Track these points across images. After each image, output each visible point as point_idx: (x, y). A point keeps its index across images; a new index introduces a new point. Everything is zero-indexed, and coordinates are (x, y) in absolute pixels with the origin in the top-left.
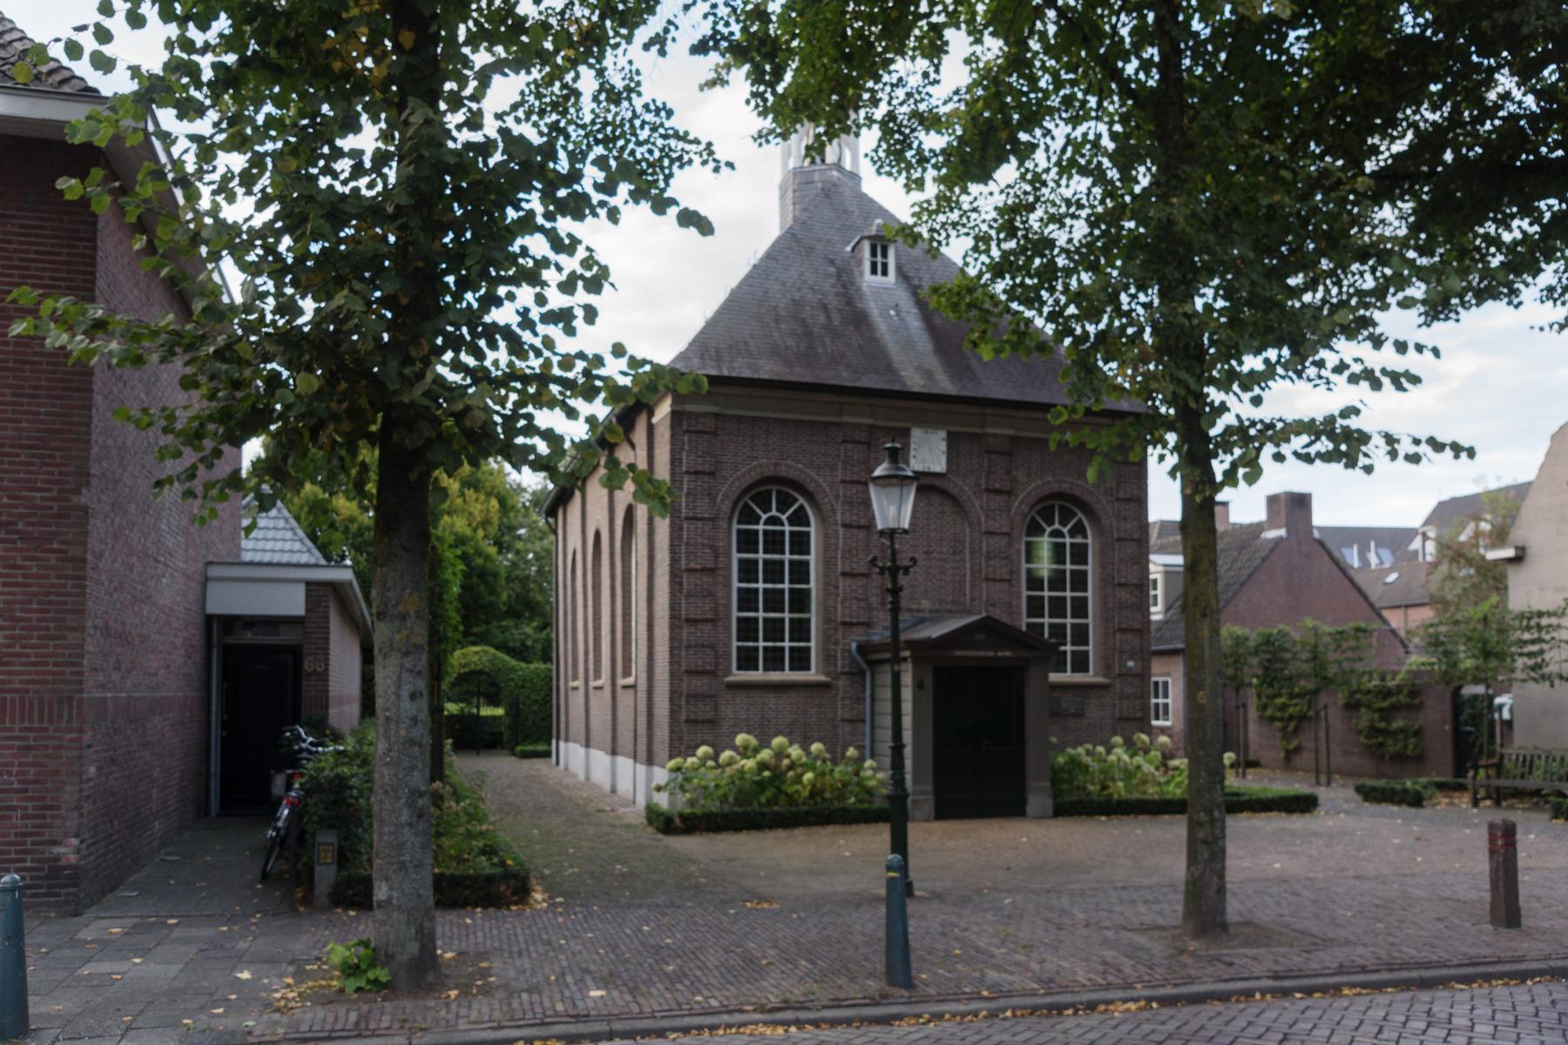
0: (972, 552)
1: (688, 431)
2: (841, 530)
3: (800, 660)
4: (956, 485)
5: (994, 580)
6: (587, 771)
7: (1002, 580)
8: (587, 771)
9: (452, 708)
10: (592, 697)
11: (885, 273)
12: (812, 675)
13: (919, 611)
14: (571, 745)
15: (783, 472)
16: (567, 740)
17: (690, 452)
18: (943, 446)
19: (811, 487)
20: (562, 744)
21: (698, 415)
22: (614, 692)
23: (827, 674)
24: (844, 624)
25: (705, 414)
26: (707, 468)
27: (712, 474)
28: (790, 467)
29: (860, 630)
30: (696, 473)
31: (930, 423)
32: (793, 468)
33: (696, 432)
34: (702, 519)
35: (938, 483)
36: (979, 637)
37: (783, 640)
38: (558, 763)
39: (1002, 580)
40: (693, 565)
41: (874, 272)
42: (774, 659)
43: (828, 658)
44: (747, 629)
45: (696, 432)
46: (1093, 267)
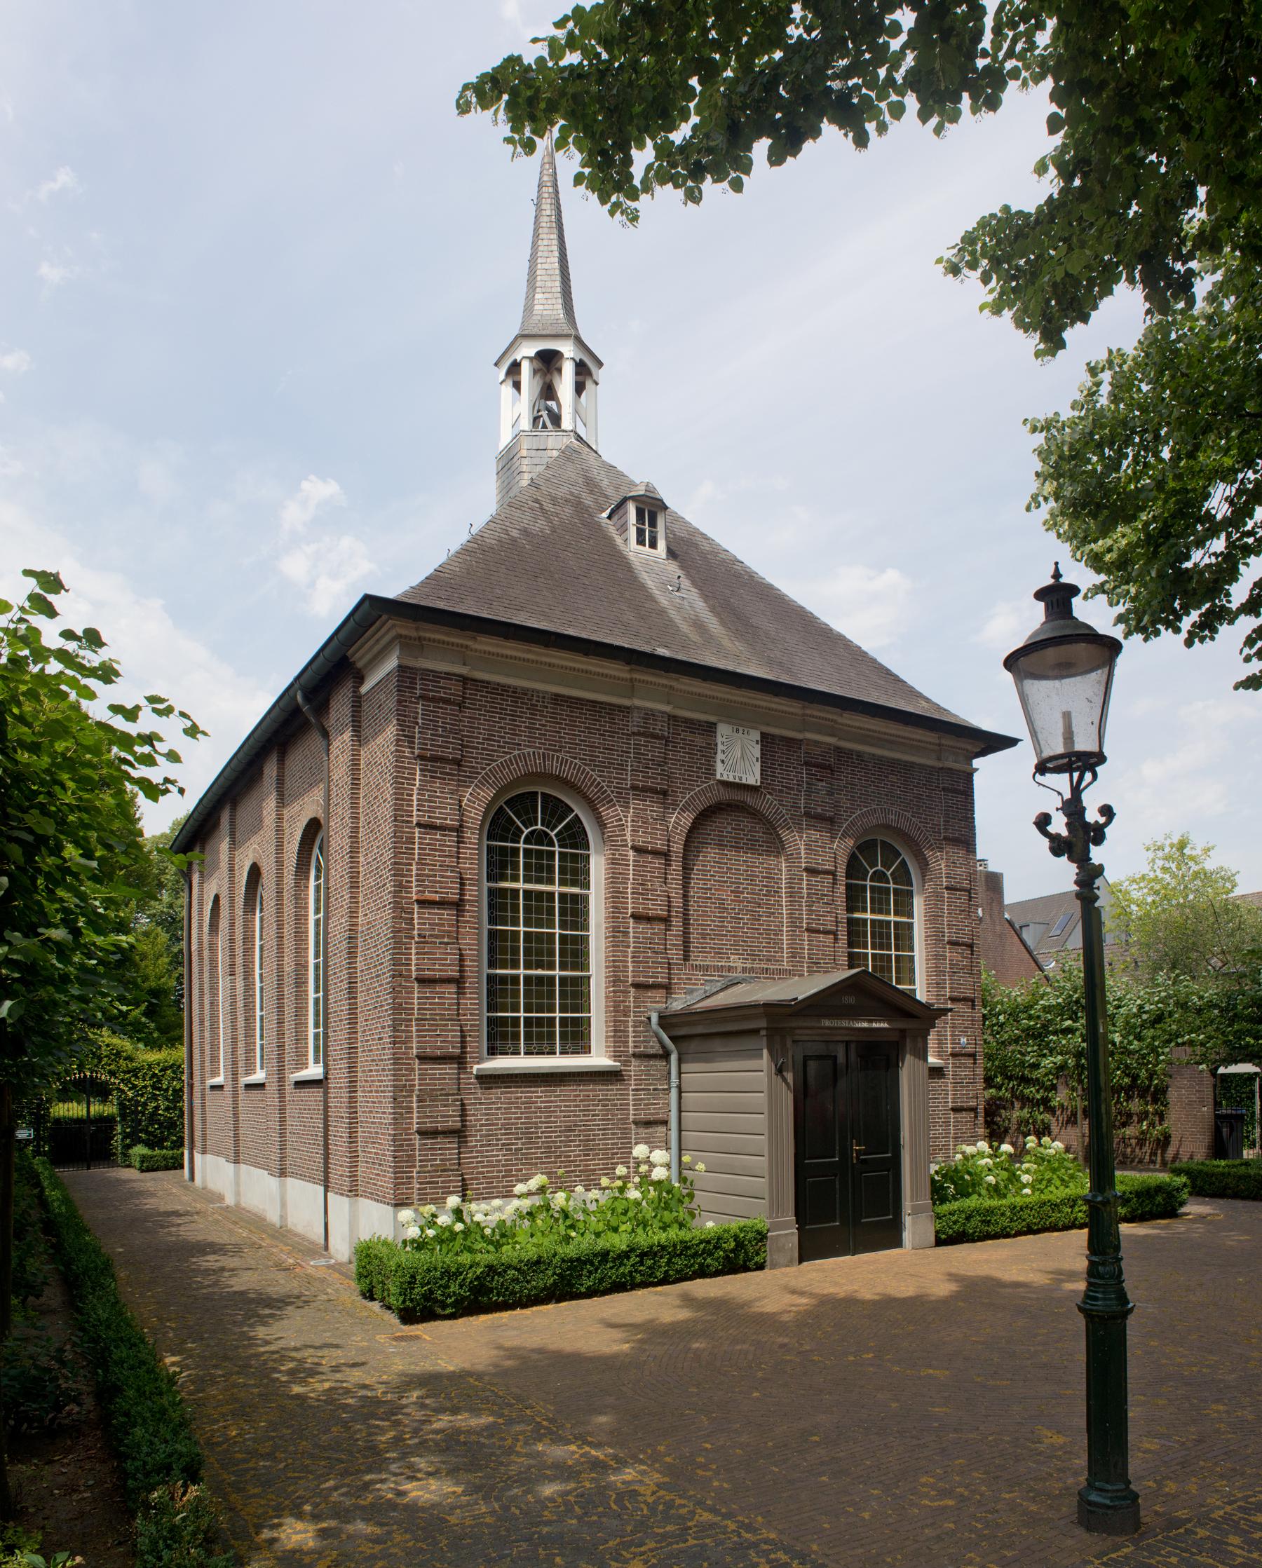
0: (791, 894)
1: (423, 697)
2: (631, 853)
3: (576, 1038)
4: (767, 804)
5: (818, 932)
6: (238, 1194)
7: (826, 932)
8: (238, 1194)
9: (1157, 1166)
10: (241, 1097)
11: (653, 545)
12: (598, 1058)
13: (730, 969)
14: (209, 1157)
15: (554, 767)
16: (204, 1152)
17: (425, 727)
18: (756, 751)
19: (592, 792)
20: (198, 1157)
21: (438, 676)
22: (281, 1089)
23: (616, 1057)
24: (637, 986)
25: (449, 676)
26: (451, 753)
27: (458, 763)
28: (563, 762)
29: (659, 994)
30: (434, 759)
31: (740, 718)
32: (565, 764)
33: (434, 700)
34: (441, 828)
35: (749, 799)
36: (848, 1000)
37: (555, 1012)
38: (192, 1178)
39: (826, 932)
40: (428, 896)
41: (641, 541)
42: (540, 1041)
43: (617, 1034)
44: (498, 990)
45: (434, 700)
46: (1122, 400)
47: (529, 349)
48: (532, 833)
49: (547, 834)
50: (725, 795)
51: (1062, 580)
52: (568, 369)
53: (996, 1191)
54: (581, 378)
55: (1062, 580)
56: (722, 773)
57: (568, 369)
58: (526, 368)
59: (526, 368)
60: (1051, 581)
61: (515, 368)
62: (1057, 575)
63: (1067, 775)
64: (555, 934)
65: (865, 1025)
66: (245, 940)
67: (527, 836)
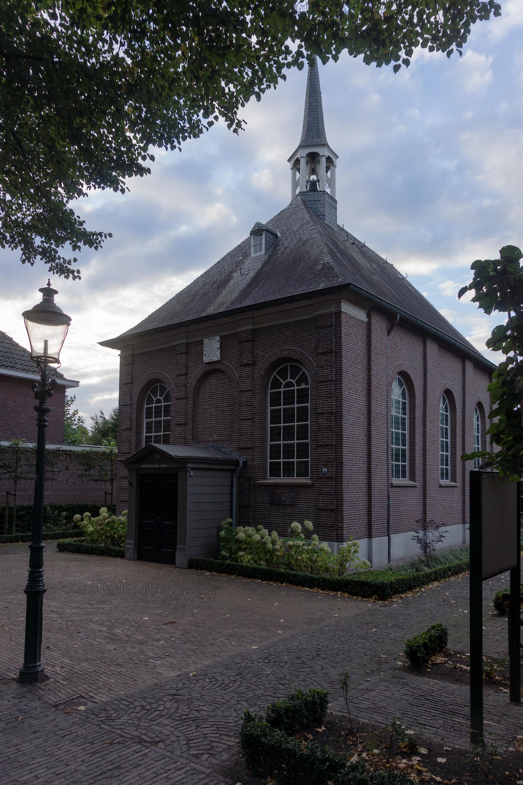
31: (210, 334)
35: (217, 366)
47: (304, 153)
48: (286, 383)
49: (292, 382)
50: (208, 368)
51: (51, 287)
52: (323, 161)
53: (493, 468)
54: (328, 164)
55: (51, 287)
56: (206, 360)
57: (323, 161)
58: (303, 162)
59: (303, 162)
60: (47, 286)
61: (297, 161)
62: (49, 284)
63: (506, 313)
64: (297, 425)
65: (158, 466)
66: (455, 428)
67: (284, 385)
